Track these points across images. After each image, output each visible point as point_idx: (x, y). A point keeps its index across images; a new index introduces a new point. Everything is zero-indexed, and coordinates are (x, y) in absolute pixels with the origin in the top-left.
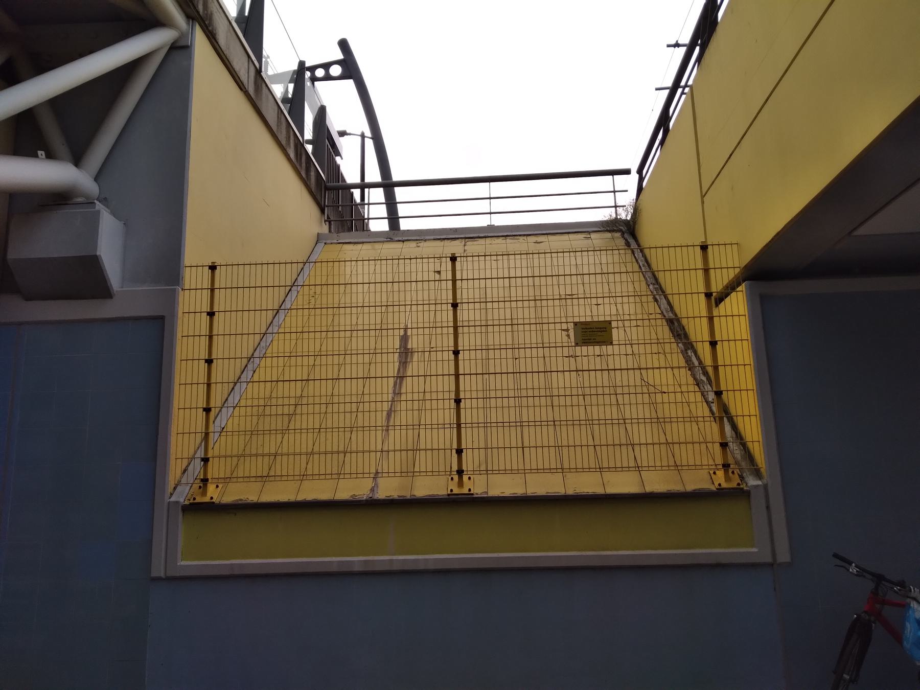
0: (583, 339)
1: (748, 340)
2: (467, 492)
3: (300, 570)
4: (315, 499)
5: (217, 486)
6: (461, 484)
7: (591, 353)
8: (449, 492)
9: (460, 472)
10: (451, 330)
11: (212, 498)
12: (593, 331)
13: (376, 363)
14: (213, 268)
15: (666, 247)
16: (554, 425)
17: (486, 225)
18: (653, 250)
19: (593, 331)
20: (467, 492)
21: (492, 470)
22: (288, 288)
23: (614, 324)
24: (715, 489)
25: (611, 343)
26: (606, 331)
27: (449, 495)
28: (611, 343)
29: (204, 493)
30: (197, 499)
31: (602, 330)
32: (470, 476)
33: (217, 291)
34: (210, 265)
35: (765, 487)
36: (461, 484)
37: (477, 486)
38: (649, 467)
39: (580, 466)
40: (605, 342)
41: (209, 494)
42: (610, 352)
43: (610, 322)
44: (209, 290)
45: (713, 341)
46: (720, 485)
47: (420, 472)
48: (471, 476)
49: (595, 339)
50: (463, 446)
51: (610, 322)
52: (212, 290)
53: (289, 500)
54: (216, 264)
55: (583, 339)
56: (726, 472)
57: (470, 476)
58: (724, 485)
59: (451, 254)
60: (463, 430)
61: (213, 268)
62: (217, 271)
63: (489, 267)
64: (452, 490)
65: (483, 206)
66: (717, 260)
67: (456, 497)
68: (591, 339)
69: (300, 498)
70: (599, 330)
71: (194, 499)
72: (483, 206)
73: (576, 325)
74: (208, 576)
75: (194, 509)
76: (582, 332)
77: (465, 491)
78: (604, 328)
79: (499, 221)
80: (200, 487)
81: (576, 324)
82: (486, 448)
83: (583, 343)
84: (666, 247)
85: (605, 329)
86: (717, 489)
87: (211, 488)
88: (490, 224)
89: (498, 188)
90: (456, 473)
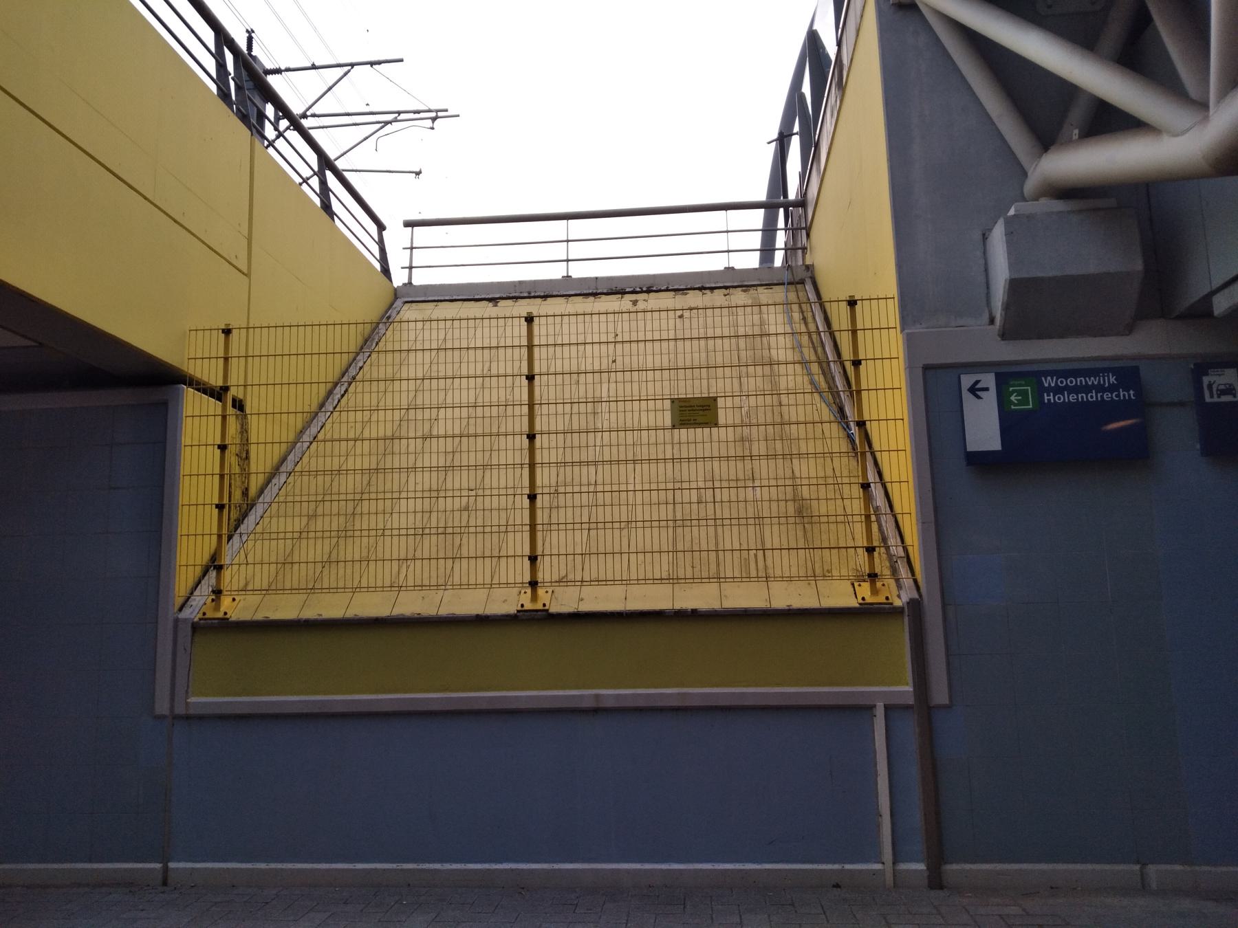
0: (681, 420)
1: (903, 420)
2: (541, 607)
3: (764, 703)
4: (402, 615)
5: (234, 600)
6: (534, 598)
7: (684, 439)
8: (520, 608)
9: (534, 584)
10: (525, 409)
11: (225, 613)
12: (693, 410)
13: (340, 456)
14: (227, 332)
15: (884, 298)
16: (716, 525)
17: (723, 269)
18: (834, 305)
19: (693, 410)
20: (885, 601)
21: (406, 587)
22: (352, 356)
23: (720, 402)
24: (857, 605)
25: (716, 425)
26: (710, 410)
27: (518, 611)
28: (716, 425)
29: (217, 608)
30: (207, 614)
31: (705, 408)
32: (234, 596)
33: (536, 350)
34: (848, 299)
35: (915, 606)
36: (534, 598)
37: (564, 601)
38: (685, 579)
39: (465, 581)
40: (707, 423)
41: (223, 609)
42: (691, 439)
43: (715, 399)
44: (850, 332)
45: (860, 421)
46: (863, 599)
47: (430, 586)
48: (236, 597)
49: (696, 420)
50: (539, 551)
51: (715, 399)
52: (226, 359)
53: (355, 615)
54: (856, 298)
55: (681, 420)
56: (873, 584)
57: (234, 596)
58: (869, 599)
59: (527, 313)
60: (539, 535)
61: (227, 332)
62: (858, 307)
63: (570, 330)
64: (522, 606)
65: (719, 242)
66: (867, 318)
67: (869, 606)
68: (690, 420)
69: (350, 614)
70: (701, 408)
71: (204, 614)
72: (719, 242)
73: (673, 402)
74: (744, 706)
75: (202, 628)
76: (680, 411)
77: (539, 606)
78: (707, 406)
79: (579, 271)
80: (213, 600)
81: (673, 401)
82: (717, 551)
83: (681, 424)
84: (884, 298)
85: (708, 408)
86: (860, 604)
87: (226, 602)
88: (727, 266)
89: (579, 228)
90: (528, 585)
